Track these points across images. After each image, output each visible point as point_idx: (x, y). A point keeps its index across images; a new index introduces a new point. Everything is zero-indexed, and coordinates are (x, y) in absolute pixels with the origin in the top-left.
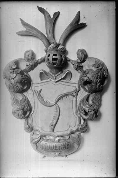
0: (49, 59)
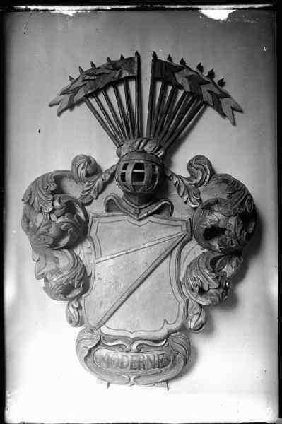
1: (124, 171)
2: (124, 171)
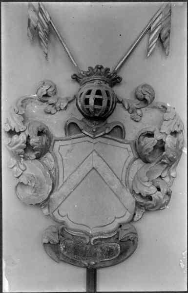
1: (87, 97)
2: (87, 97)
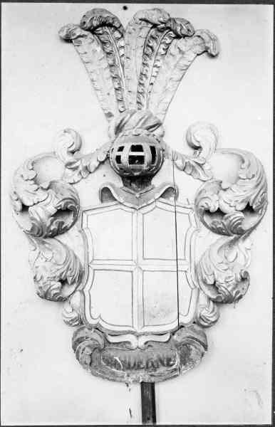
0: (118, 159)
1: (119, 153)
